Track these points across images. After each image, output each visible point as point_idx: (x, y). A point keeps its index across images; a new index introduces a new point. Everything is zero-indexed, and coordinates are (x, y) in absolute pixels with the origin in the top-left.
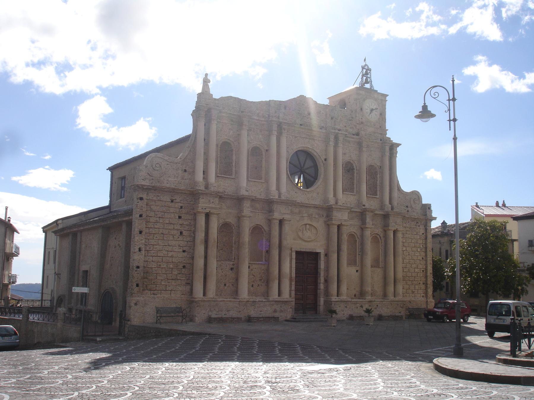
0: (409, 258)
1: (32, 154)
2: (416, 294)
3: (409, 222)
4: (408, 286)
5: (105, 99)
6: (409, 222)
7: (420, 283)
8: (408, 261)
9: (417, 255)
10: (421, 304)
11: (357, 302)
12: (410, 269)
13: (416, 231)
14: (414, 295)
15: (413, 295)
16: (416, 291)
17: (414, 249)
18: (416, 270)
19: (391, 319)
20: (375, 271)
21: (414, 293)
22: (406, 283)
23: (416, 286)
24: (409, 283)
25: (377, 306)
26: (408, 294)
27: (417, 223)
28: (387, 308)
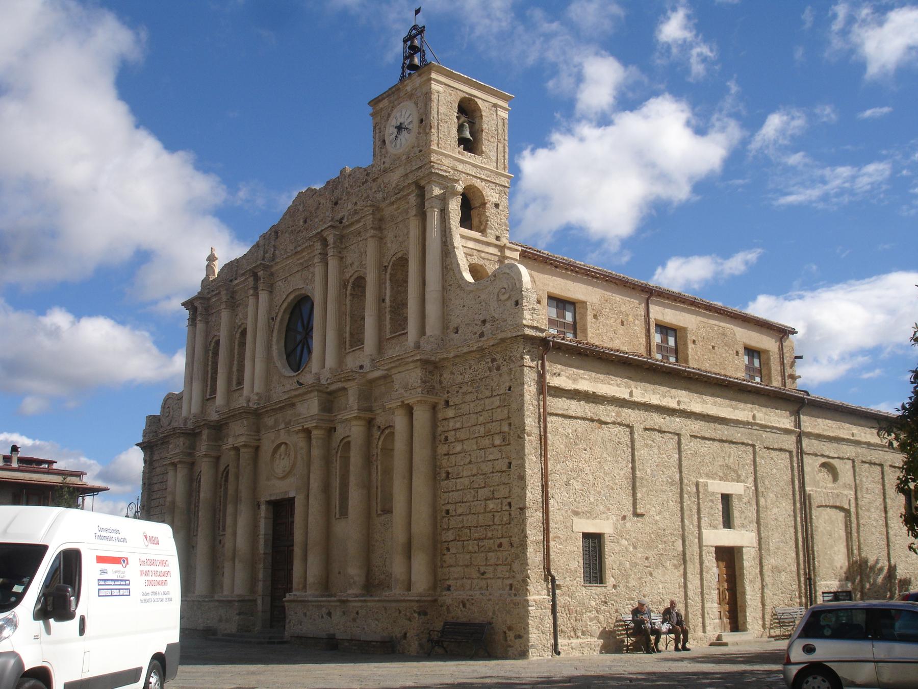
0: (472, 470)
1: (868, 113)
2: (489, 581)
3: (470, 368)
4: (468, 556)
5: (526, 153)
6: (470, 368)
7: (500, 545)
8: (466, 481)
9: (491, 457)
10: (494, 611)
11: (322, 604)
12: (473, 504)
13: (490, 387)
14: (484, 582)
15: (483, 583)
16: (491, 569)
17: (486, 442)
18: (491, 505)
19: (354, 648)
20: (388, 524)
21: (484, 577)
22: (463, 547)
23: (490, 554)
24: (470, 548)
25: (357, 613)
26: (469, 581)
27: (493, 360)
28: (377, 620)
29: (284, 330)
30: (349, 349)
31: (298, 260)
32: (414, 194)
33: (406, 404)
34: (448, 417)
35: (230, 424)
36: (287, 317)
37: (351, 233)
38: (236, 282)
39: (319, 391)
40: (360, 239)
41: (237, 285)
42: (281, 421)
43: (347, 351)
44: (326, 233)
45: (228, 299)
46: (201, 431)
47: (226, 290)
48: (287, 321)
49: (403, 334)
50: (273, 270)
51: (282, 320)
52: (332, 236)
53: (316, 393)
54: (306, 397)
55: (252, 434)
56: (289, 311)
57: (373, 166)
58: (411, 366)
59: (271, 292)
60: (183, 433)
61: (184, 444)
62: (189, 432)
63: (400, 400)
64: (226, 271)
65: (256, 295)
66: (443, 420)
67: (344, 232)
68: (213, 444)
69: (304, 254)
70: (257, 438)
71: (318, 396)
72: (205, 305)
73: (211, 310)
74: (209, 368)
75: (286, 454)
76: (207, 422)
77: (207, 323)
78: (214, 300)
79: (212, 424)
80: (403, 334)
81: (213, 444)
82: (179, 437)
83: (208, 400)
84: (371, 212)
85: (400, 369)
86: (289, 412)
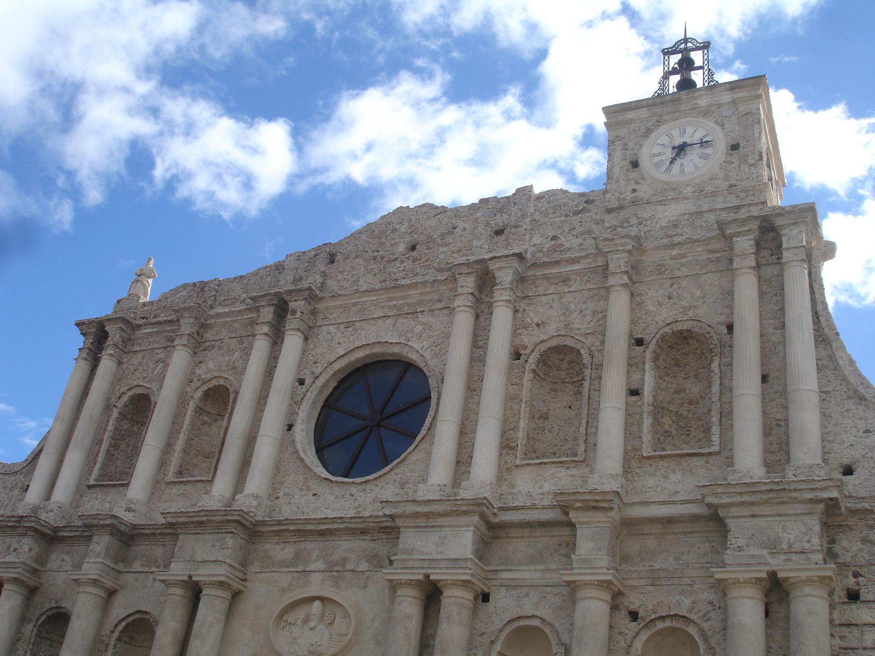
29: (321, 404)
30: (522, 459)
31: (390, 300)
32: (752, 237)
33: (194, 582)
34: (859, 622)
35: (181, 537)
36: (334, 384)
37: (546, 277)
38: (220, 310)
39: (482, 516)
40: (566, 289)
41: (218, 315)
42: (314, 556)
43: (518, 462)
44: (498, 265)
45: (193, 333)
46: (91, 536)
47: (196, 318)
48: (331, 389)
49: (123, 485)
50: (321, 306)
51: (324, 386)
52: (510, 272)
53: (476, 519)
54: (439, 521)
55: (236, 565)
56: (341, 376)
57: (605, 192)
58: (798, 508)
59: (306, 339)
60: (36, 530)
61: (30, 550)
62: (48, 531)
63: (424, 571)
64: (184, 293)
65: (277, 339)
66: (840, 625)
67: (530, 273)
68: (108, 563)
69: (410, 293)
70: (241, 576)
71: (476, 527)
72: (126, 336)
73: (133, 345)
74: (107, 434)
75: (321, 620)
76: (116, 522)
77: (120, 363)
78: (148, 331)
79: (123, 528)
80: (123, 485)
81: (108, 563)
82: (25, 535)
83: (90, 487)
84: (629, 247)
85: (767, 510)
86: (343, 543)
